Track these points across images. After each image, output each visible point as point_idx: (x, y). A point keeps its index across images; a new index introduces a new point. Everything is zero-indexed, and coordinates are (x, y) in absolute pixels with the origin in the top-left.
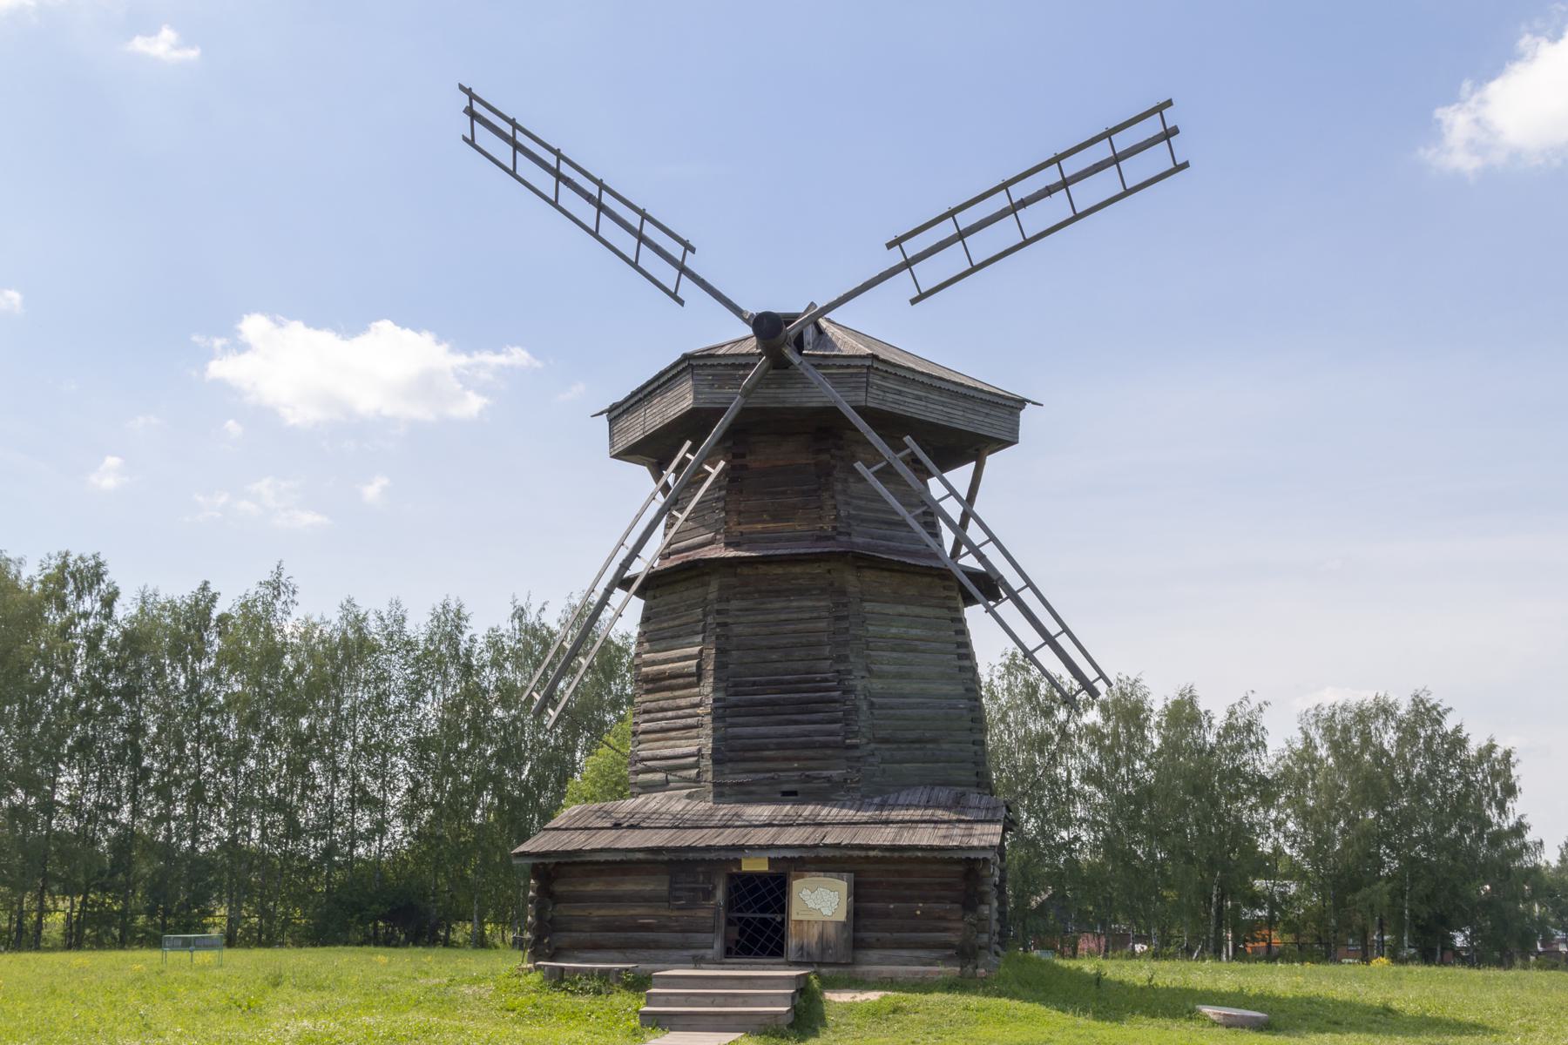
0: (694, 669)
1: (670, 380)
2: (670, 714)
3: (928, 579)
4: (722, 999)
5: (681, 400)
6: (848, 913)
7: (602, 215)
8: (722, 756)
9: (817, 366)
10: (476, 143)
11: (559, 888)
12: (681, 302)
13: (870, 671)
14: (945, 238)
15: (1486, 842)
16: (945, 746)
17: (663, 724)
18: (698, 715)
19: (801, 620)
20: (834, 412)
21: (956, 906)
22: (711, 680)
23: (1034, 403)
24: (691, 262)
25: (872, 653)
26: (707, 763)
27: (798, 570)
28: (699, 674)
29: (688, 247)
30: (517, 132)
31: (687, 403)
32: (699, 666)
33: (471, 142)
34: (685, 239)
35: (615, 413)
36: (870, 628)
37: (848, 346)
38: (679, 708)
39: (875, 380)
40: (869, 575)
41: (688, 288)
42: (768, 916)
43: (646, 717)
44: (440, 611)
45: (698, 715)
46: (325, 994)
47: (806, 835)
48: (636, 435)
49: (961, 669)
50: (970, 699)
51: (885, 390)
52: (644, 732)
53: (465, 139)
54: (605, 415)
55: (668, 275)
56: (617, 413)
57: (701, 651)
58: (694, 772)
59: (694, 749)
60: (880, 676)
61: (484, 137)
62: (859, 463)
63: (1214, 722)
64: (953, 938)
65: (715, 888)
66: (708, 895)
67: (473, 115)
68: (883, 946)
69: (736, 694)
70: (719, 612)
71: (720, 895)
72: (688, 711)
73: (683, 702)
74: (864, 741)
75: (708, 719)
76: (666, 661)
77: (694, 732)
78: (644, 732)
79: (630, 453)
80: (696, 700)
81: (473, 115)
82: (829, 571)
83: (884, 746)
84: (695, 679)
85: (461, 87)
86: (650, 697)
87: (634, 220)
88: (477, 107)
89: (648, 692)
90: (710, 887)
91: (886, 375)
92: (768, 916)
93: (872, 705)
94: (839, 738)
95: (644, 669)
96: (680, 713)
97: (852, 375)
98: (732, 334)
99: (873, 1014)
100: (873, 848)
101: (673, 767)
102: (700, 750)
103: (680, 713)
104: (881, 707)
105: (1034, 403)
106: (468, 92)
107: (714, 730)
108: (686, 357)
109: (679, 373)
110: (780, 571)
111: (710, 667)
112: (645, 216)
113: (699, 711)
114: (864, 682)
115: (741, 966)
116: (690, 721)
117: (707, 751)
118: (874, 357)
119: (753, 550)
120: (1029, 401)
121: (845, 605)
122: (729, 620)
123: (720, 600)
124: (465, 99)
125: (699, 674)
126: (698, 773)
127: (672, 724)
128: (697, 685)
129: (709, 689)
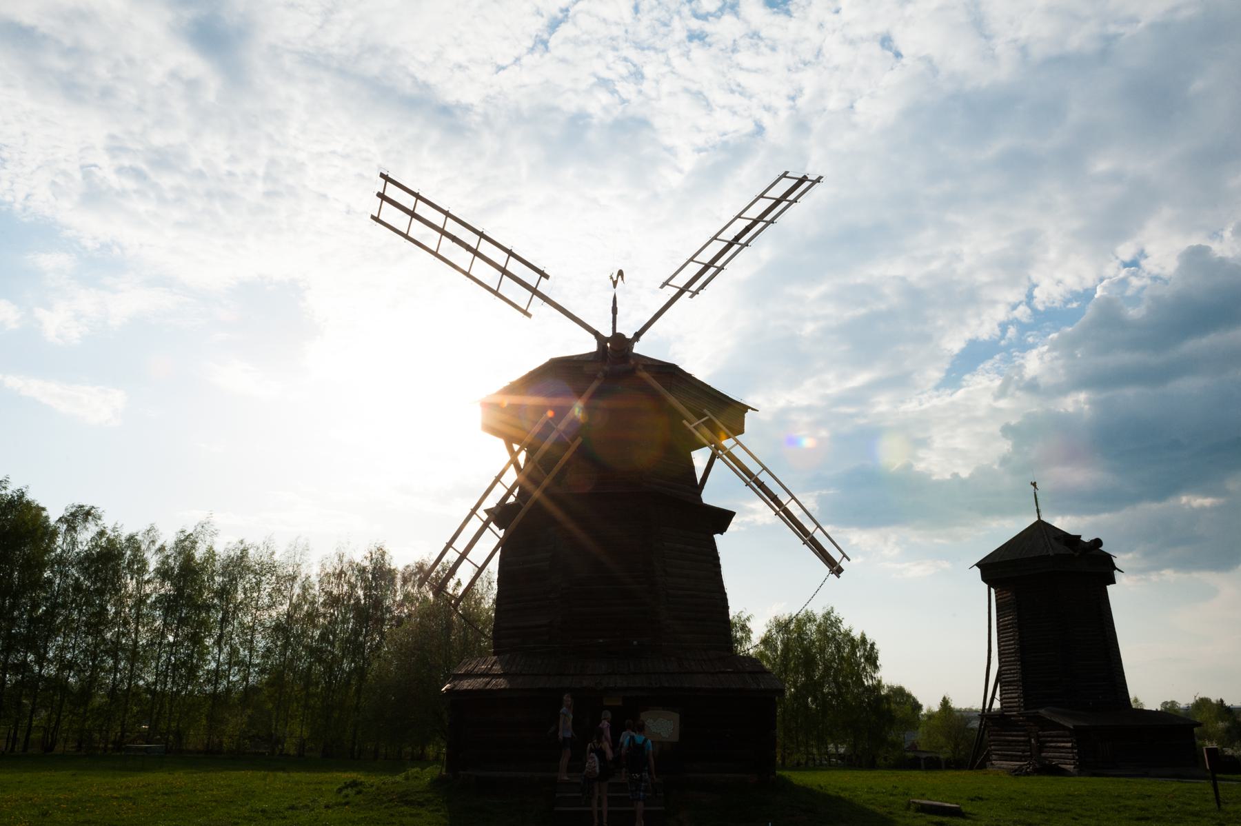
7: (670, 283)
10: (761, 199)
14: (708, 504)
15: (320, 686)
23: (753, 409)
29: (543, 274)
30: (788, 203)
33: (785, 175)
34: (494, 478)
44: (300, 550)
46: (294, 811)
53: (787, 172)
61: (786, 184)
63: (1036, 292)
67: (801, 181)
81: (801, 181)
85: (820, 178)
88: (806, 184)
99: (998, 775)
105: (753, 409)
106: (818, 180)
120: (750, 408)
124: (814, 178)
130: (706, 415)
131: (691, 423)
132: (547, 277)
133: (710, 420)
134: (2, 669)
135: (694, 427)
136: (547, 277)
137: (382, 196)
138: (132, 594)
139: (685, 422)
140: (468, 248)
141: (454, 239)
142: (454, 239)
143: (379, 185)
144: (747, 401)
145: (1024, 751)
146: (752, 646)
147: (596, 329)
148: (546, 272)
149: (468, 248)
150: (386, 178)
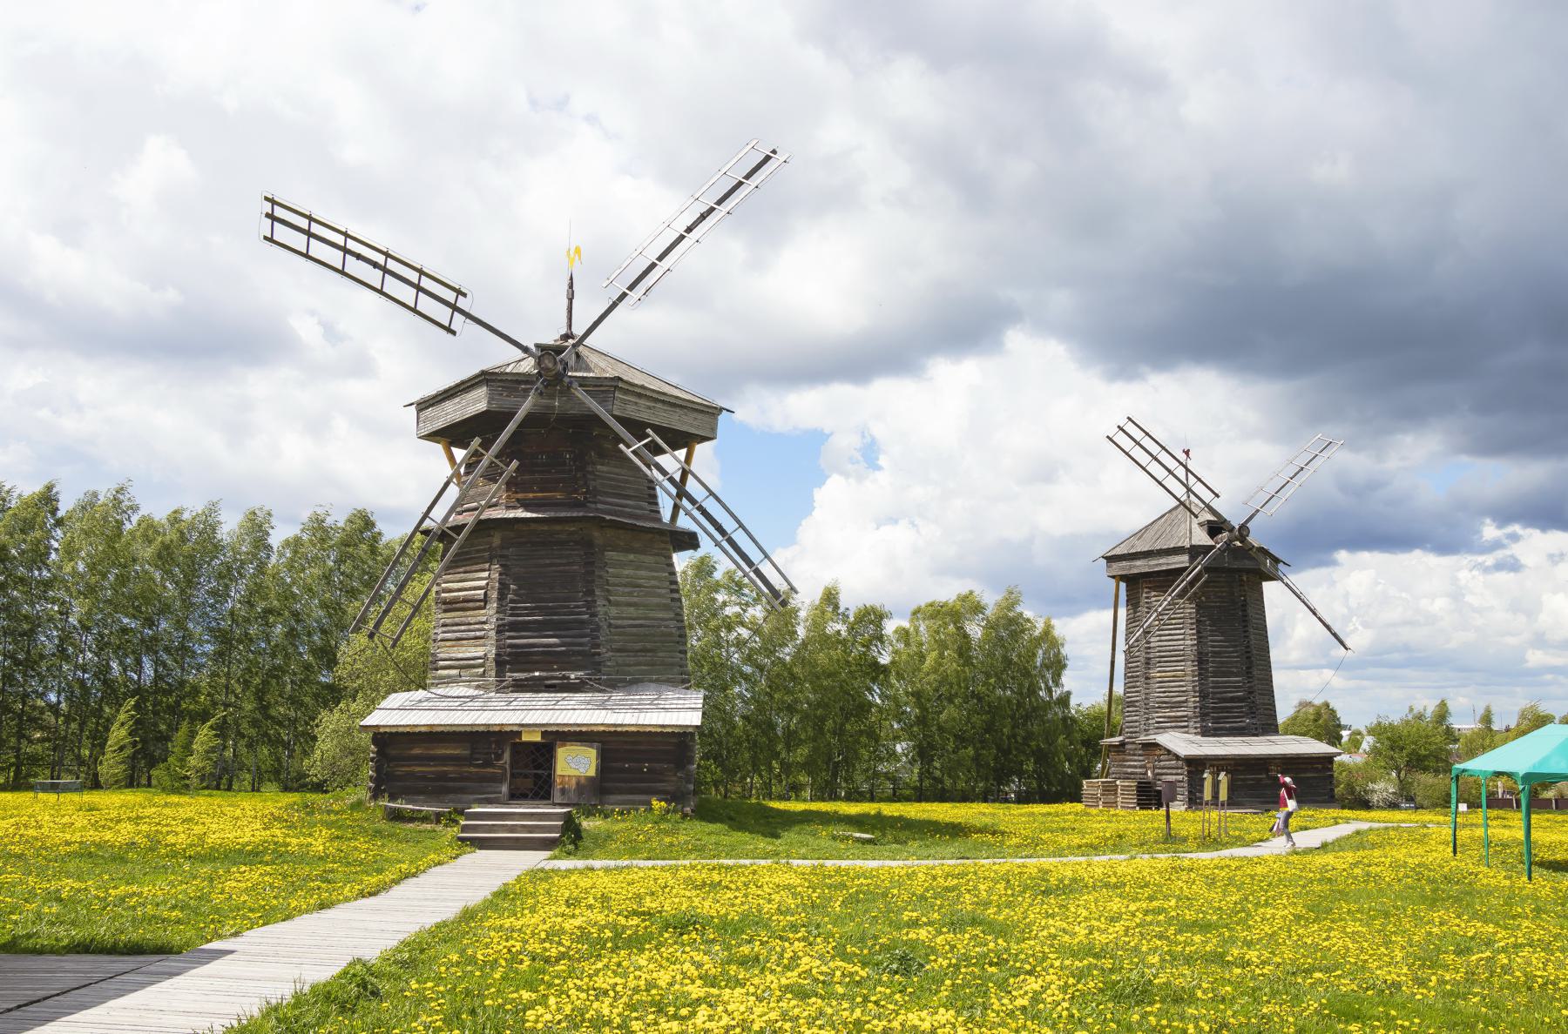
0: (482, 597)
1: (468, 387)
2: (463, 628)
3: (650, 536)
4: (519, 829)
5: (476, 402)
6: (597, 770)
8: (502, 663)
9: (581, 386)
11: (393, 752)
12: (454, 333)
13: (609, 601)
16: (661, 654)
17: (458, 635)
18: (484, 630)
19: (560, 565)
20: (595, 419)
21: (672, 765)
22: (495, 605)
24: (462, 303)
25: (610, 588)
26: (491, 664)
27: (558, 527)
28: (486, 600)
29: (459, 292)
31: (482, 406)
32: (485, 594)
35: (423, 406)
36: (610, 570)
37: (601, 369)
38: (471, 624)
39: (617, 394)
40: (610, 533)
41: (459, 321)
42: (540, 772)
43: (444, 629)
45: (484, 630)
47: (388, 718)
48: (439, 424)
49: (673, 600)
50: (678, 621)
51: (625, 402)
52: (442, 640)
54: (414, 406)
55: (442, 314)
56: (424, 405)
57: (487, 584)
58: (482, 670)
59: (481, 654)
60: (617, 604)
62: (518, 463)
64: (669, 787)
65: (503, 752)
66: (499, 757)
68: (621, 792)
69: (511, 615)
70: (501, 556)
71: (507, 756)
72: (477, 626)
73: (472, 620)
74: (604, 650)
75: (492, 634)
76: (466, 589)
77: (482, 641)
78: (442, 640)
79: (433, 436)
80: (484, 619)
82: (581, 529)
83: (618, 654)
84: (482, 604)
86: (449, 615)
87: (413, 276)
89: (446, 611)
90: (500, 751)
91: (626, 392)
92: (540, 772)
93: (610, 625)
94: (587, 648)
95: (443, 595)
96: (472, 627)
97: (603, 391)
98: (502, 357)
100: (400, 726)
101: (465, 665)
102: (485, 655)
103: (472, 627)
104: (617, 627)
105: (728, 411)
107: (497, 641)
108: (483, 373)
109: (477, 383)
110: (546, 528)
111: (494, 595)
112: (421, 272)
113: (486, 627)
114: (605, 609)
115: (520, 806)
116: (478, 634)
117: (492, 656)
118: (619, 379)
119: (544, 512)
121: (593, 554)
122: (509, 563)
123: (502, 547)
125: (486, 600)
126: (484, 671)
127: (464, 635)
128: (484, 608)
129: (492, 612)
130: (648, 436)
131: (628, 446)
132: (465, 295)
133: (653, 441)
134: (1389, 1031)
135: (633, 452)
136: (465, 295)
137: (271, 216)
138: (58, 646)
139: (622, 446)
140: (375, 265)
141: (359, 257)
142: (359, 257)
143: (268, 207)
144: (721, 403)
145: (1052, 822)
146: (1488, 521)
147: (476, 371)
148: (463, 290)
149: (375, 265)
150: (273, 202)
